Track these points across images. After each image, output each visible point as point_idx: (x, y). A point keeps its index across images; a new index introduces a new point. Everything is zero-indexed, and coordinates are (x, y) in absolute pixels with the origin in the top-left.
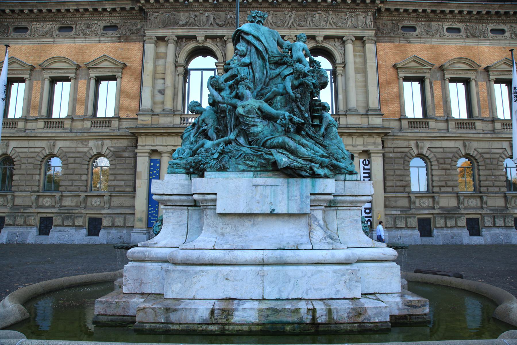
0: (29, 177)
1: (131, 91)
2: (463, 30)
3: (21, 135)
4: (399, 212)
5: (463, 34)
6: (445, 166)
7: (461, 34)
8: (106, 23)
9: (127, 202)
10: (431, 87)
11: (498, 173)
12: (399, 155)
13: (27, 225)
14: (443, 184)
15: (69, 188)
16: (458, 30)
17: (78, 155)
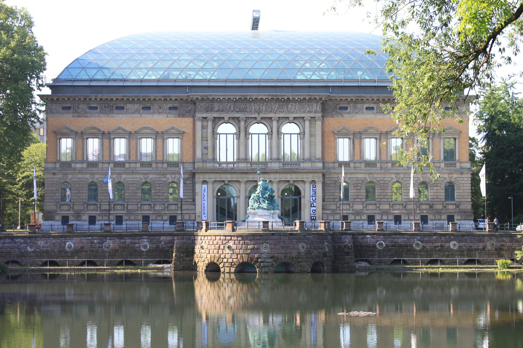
0: (135, 194)
1: (188, 147)
2: (375, 108)
3: (129, 171)
4: (330, 212)
5: (375, 111)
6: (357, 188)
8: (171, 105)
9: (192, 207)
11: (387, 191)
12: (332, 182)
13: (137, 220)
14: (356, 197)
15: (157, 200)
16: (372, 108)
17: (161, 182)
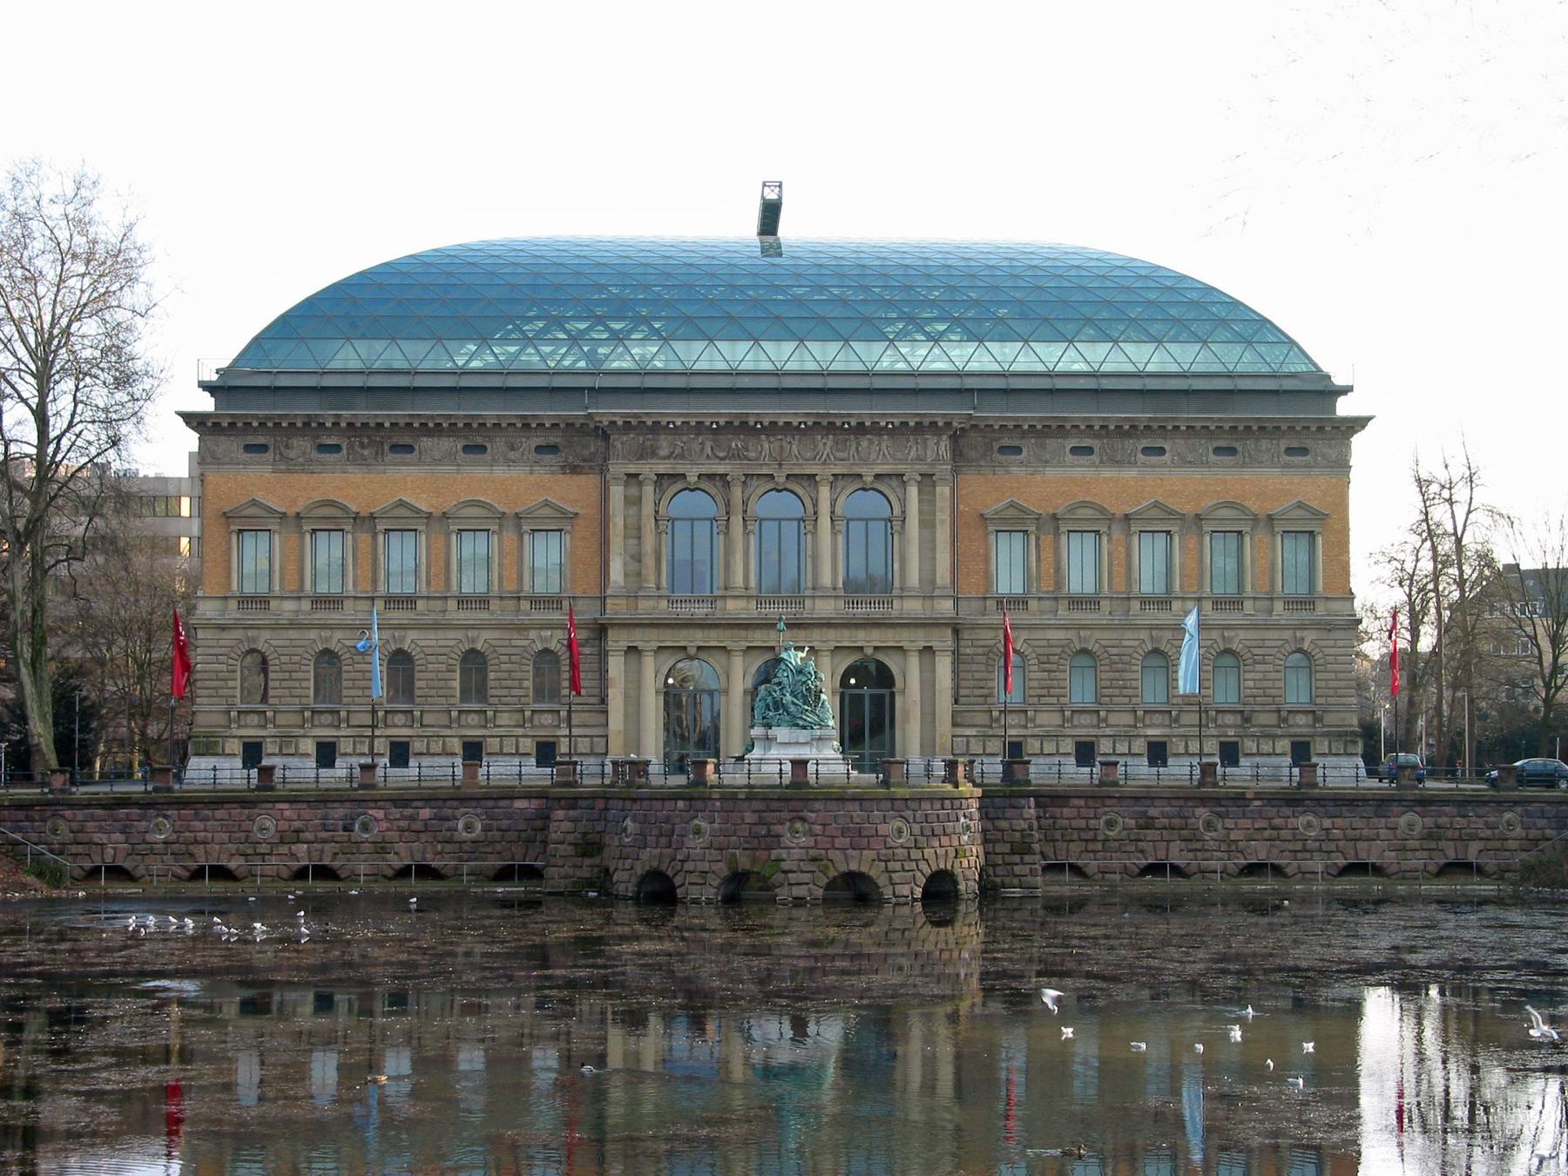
0: (442, 683)
2: (1096, 450)
7: (1093, 457)
8: (541, 441)
10: (1037, 546)
12: (980, 650)
17: (514, 651)
